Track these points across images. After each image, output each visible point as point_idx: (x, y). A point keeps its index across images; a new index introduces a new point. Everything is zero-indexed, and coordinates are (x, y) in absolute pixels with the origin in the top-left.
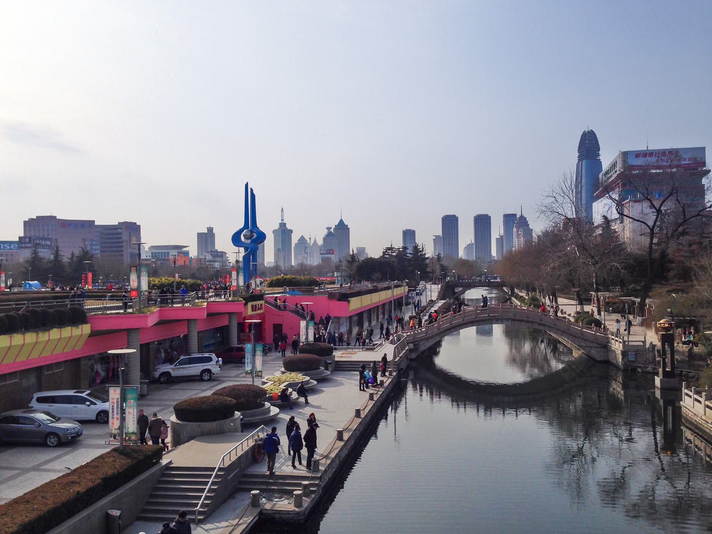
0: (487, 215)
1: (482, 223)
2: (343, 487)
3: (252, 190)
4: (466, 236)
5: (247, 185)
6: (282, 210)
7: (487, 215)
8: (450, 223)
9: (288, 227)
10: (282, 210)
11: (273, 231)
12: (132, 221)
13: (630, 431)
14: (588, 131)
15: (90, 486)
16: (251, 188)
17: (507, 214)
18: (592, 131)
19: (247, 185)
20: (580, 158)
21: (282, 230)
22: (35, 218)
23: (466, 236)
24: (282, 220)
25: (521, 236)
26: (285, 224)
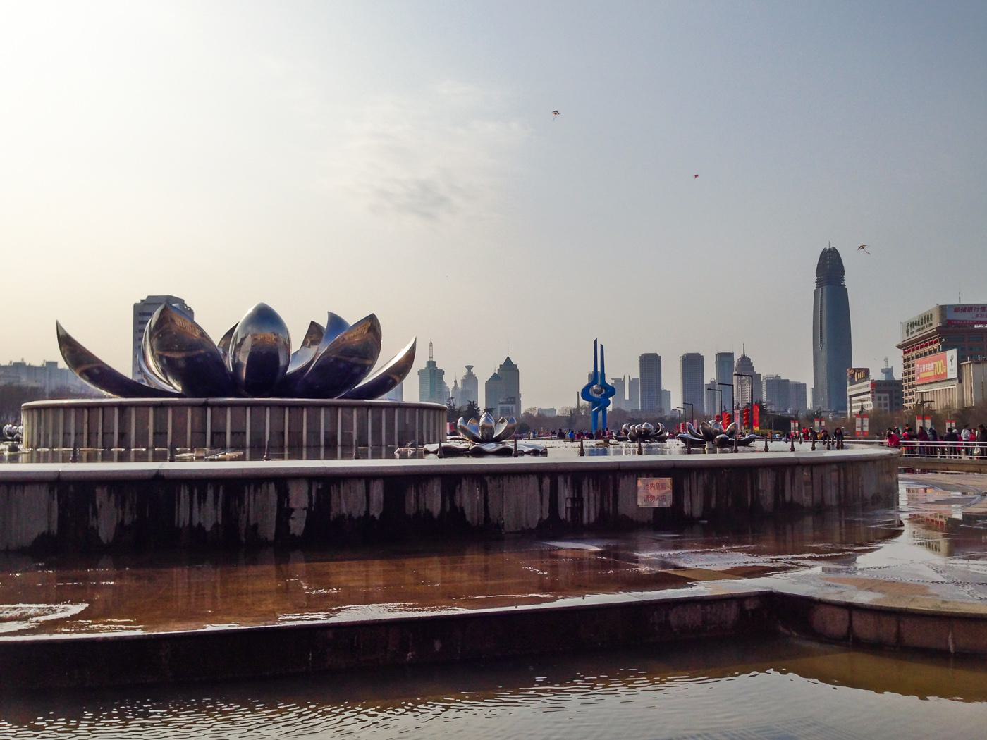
0: (698, 355)
1: (692, 364)
2: (148, 297)
3: (602, 346)
4: (672, 381)
5: (596, 341)
6: (431, 345)
7: (698, 355)
8: (650, 364)
9: (439, 366)
10: (431, 345)
11: (419, 372)
12: (154, 295)
13: (850, 627)
14: (829, 249)
15: (179, 570)
16: (602, 346)
17: (721, 353)
18: (834, 249)
19: (596, 341)
20: (820, 283)
21: (430, 371)
22: (140, 302)
23: (672, 381)
24: (431, 357)
25: (745, 382)
26: (435, 362)
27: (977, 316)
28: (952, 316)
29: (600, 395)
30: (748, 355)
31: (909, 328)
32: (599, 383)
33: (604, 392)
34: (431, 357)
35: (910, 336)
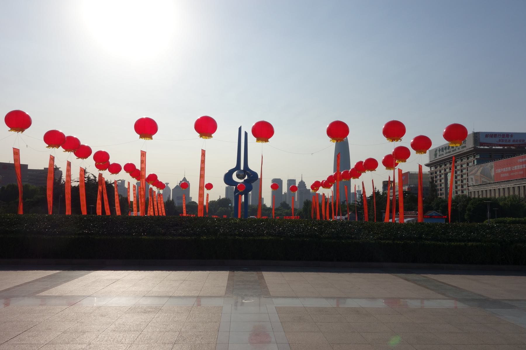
5: (240, 129)
6: (203, 153)
10: (203, 153)
19: (240, 129)
27: (500, 141)
28: (483, 140)
29: (243, 181)
30: (304, 180)
31: (438, 152)
32: (242, 168)
35: (438, 157)
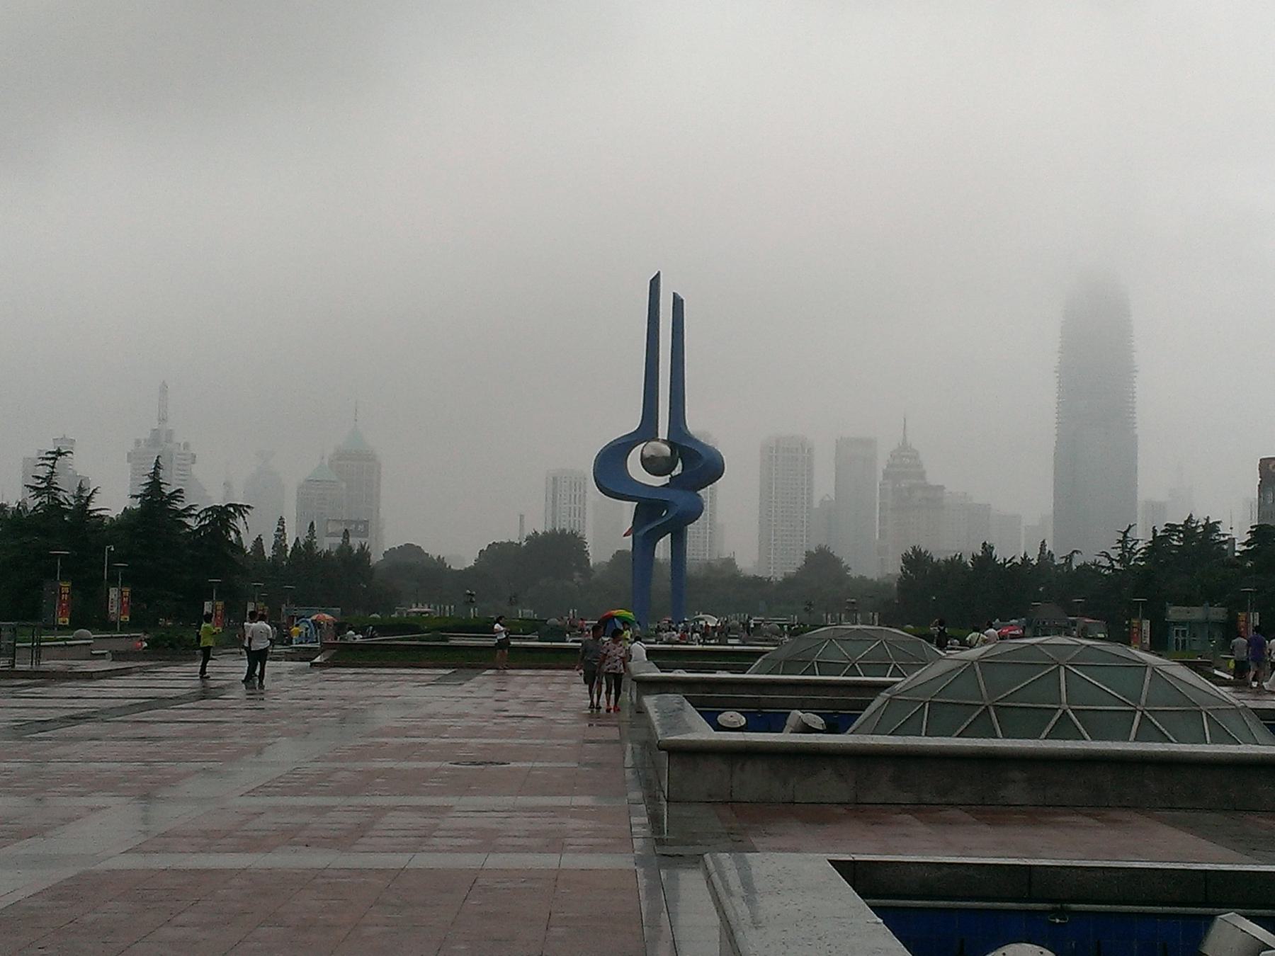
3: (678, 303)
5: (655, 283)
16: (678, 303)
19: (655, 283)
24: (163, 420)
33: (678, 470)
34: (163, 420)
